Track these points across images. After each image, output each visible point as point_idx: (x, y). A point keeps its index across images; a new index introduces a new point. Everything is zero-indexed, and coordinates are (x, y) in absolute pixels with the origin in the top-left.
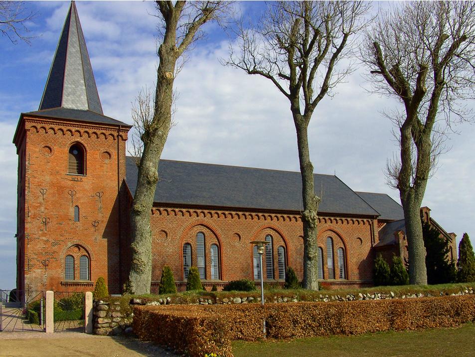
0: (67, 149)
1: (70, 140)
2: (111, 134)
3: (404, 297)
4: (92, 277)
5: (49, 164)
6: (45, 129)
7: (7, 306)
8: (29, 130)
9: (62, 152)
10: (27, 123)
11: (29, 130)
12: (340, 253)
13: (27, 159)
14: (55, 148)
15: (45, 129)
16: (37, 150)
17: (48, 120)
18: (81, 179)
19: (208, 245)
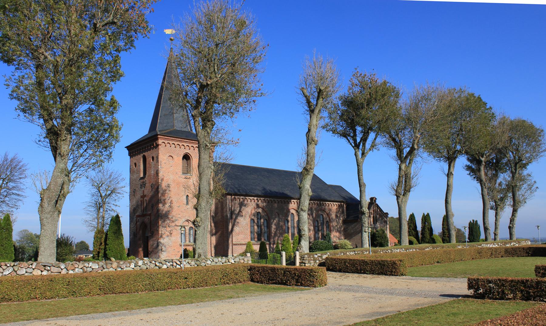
0: (181, 158)
1: (183, 152)
2: (183, 145)
3: (408, 251)
4: (22, 273)
5: (172, 167)
6: (184, 146)
7: (268, 258)
8: (160, 145)
9: (179, 160)
10: (159, 140)
11: (160, 145)
12: (309, 230)
13: (160, 164)
14: (175, 157)
15: (184, 146)
16: (165, 158)
17: (166, 137)
18: (190, 177)
19: (488, 206)
